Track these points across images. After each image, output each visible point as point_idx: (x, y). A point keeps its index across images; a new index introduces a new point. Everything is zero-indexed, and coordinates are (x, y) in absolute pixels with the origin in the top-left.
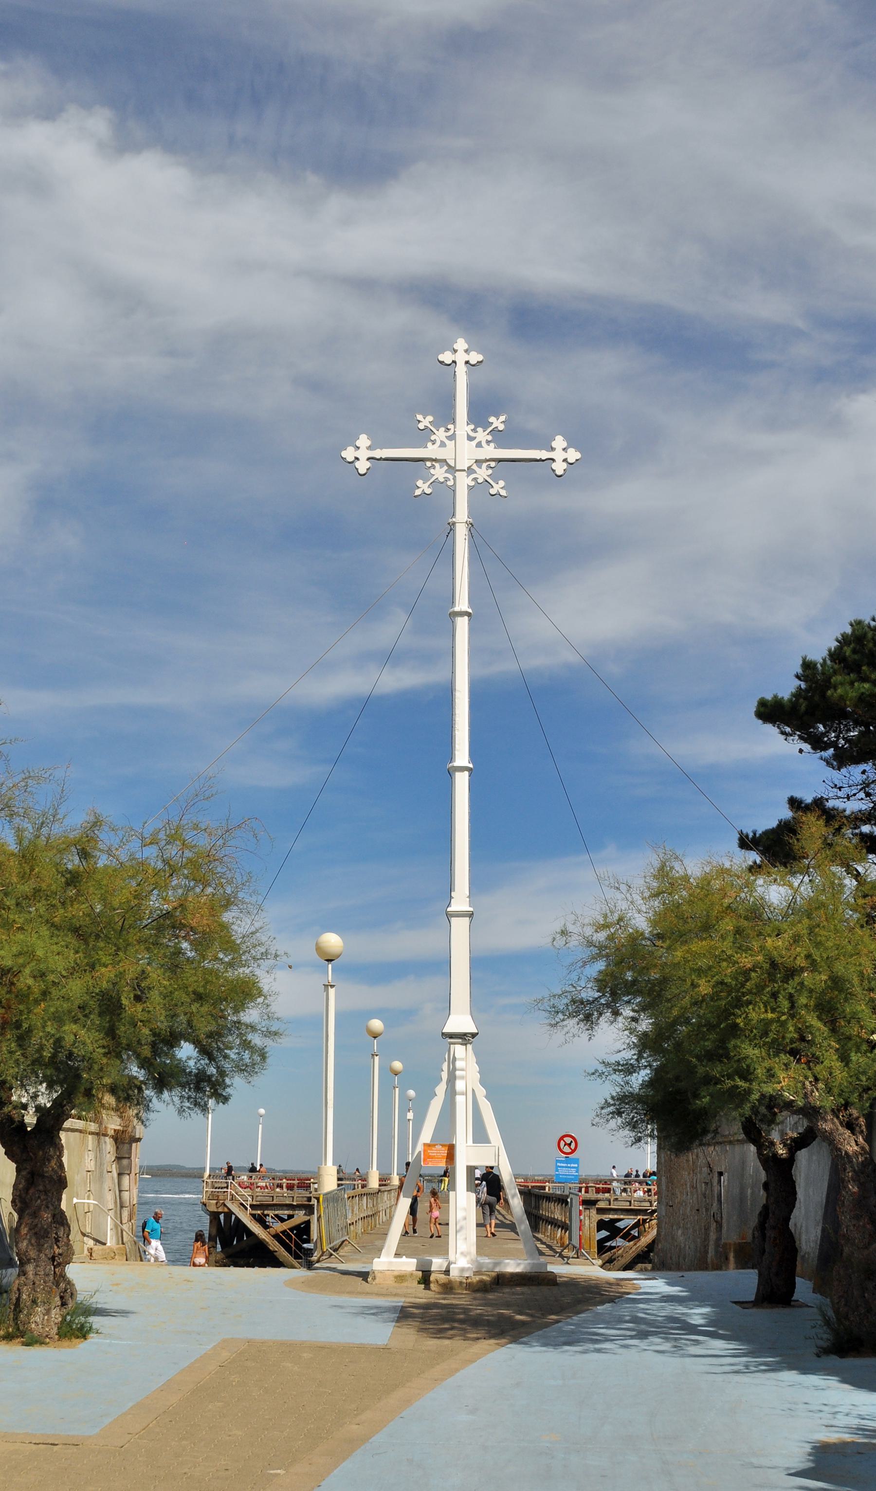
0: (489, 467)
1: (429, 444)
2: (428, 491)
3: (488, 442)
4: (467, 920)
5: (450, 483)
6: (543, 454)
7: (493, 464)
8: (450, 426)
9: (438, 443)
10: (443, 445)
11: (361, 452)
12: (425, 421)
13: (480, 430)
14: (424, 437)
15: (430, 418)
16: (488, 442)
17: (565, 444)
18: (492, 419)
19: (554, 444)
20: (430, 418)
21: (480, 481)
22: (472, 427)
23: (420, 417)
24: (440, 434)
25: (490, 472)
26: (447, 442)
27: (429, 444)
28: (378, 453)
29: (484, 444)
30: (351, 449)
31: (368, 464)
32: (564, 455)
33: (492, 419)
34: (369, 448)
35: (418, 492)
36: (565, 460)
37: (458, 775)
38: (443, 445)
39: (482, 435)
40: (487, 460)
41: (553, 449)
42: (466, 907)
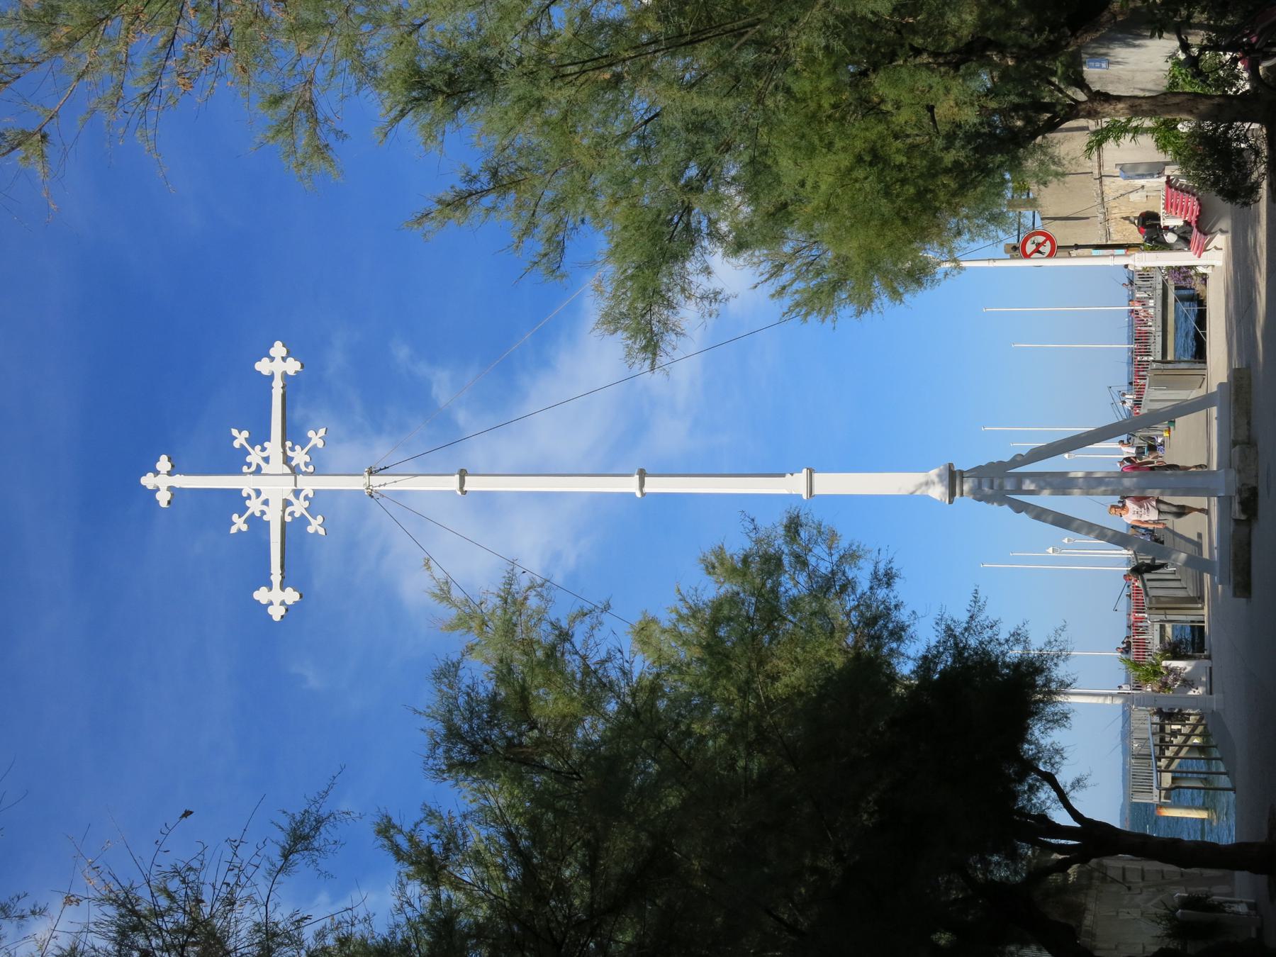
0: (292, 449)
1: (265, 518)
2: (320, 519)
3: (264, 449)
4: (816, 476)
5: (245, 469)
6: (276, 577)
7: (289, 444)
8: (311, 469)
9: (264, 508)
10: (266, 503)
11: (278, 364)
12: (239, 524)
13: (248, 459)
14: (258, 525)
15: (235, 517)
16: (264, 449)
17: (265, 360)
18: (236, 444)
19: (289, 590)
20: (235, 517)
21: (308, 459)
22: (311, 495)
23: (322, 432)
24: (254, 506)
25: (298, 448)
26: (263, 497)
27: (265, 518)
28: (276, 577)
29: (265, 454)
30: (271, 610)
31: (289, 590)
32: (278, 360)
33: (236, 444)
34: (285, 376)
35: (322, 531)
36: (284, 359)
37: (817, 491)
38: (266, 503)
39: (255, 457)
40: (284, 452)
41: (283, 588)
42: (802, 477)
